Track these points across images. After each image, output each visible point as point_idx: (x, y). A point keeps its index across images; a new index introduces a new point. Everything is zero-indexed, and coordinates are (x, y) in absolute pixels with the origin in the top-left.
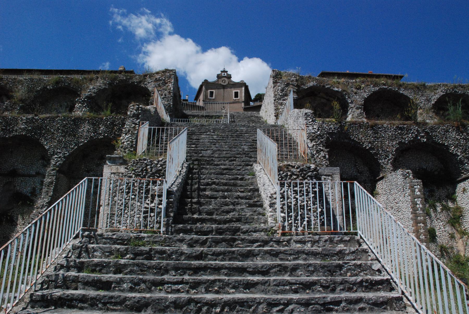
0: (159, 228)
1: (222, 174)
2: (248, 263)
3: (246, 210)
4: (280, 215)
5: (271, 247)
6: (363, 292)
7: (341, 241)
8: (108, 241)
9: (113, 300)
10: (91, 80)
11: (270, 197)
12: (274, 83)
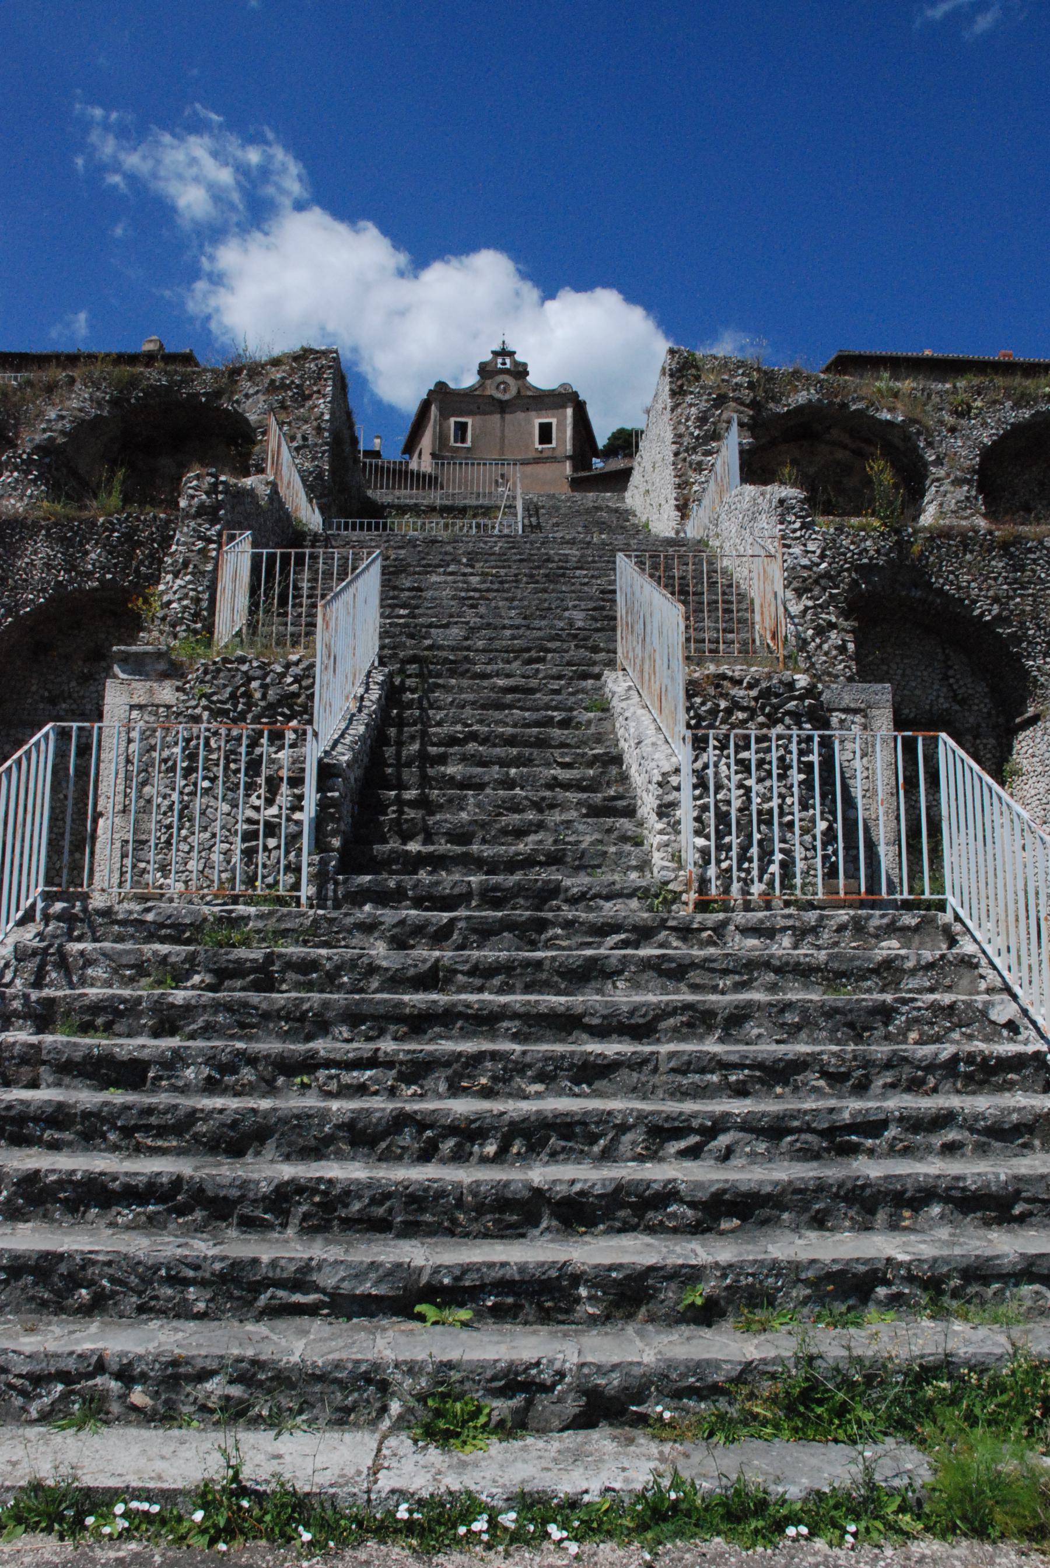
0: (296, 886)
1: (499, 706)
2: (586, 1000)
3: (581, 828)
4: (690, 843)
5: (661, 946)
6: (958, 1092)
7: (892, 929)
8: (131, 930)
9: (153, 1120)
10: (50, 388)
11: (660, 784)
12: (673, 393)
